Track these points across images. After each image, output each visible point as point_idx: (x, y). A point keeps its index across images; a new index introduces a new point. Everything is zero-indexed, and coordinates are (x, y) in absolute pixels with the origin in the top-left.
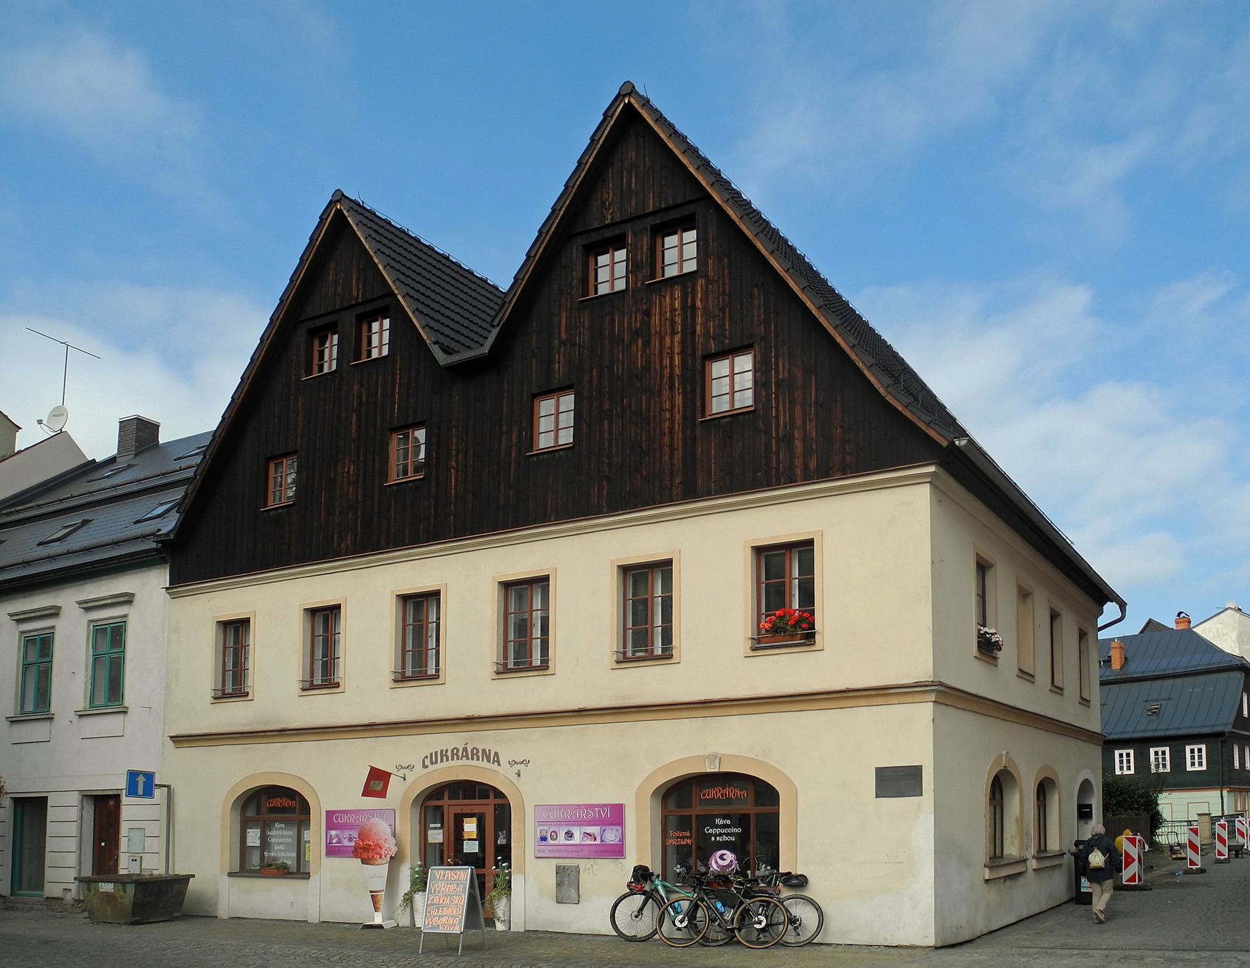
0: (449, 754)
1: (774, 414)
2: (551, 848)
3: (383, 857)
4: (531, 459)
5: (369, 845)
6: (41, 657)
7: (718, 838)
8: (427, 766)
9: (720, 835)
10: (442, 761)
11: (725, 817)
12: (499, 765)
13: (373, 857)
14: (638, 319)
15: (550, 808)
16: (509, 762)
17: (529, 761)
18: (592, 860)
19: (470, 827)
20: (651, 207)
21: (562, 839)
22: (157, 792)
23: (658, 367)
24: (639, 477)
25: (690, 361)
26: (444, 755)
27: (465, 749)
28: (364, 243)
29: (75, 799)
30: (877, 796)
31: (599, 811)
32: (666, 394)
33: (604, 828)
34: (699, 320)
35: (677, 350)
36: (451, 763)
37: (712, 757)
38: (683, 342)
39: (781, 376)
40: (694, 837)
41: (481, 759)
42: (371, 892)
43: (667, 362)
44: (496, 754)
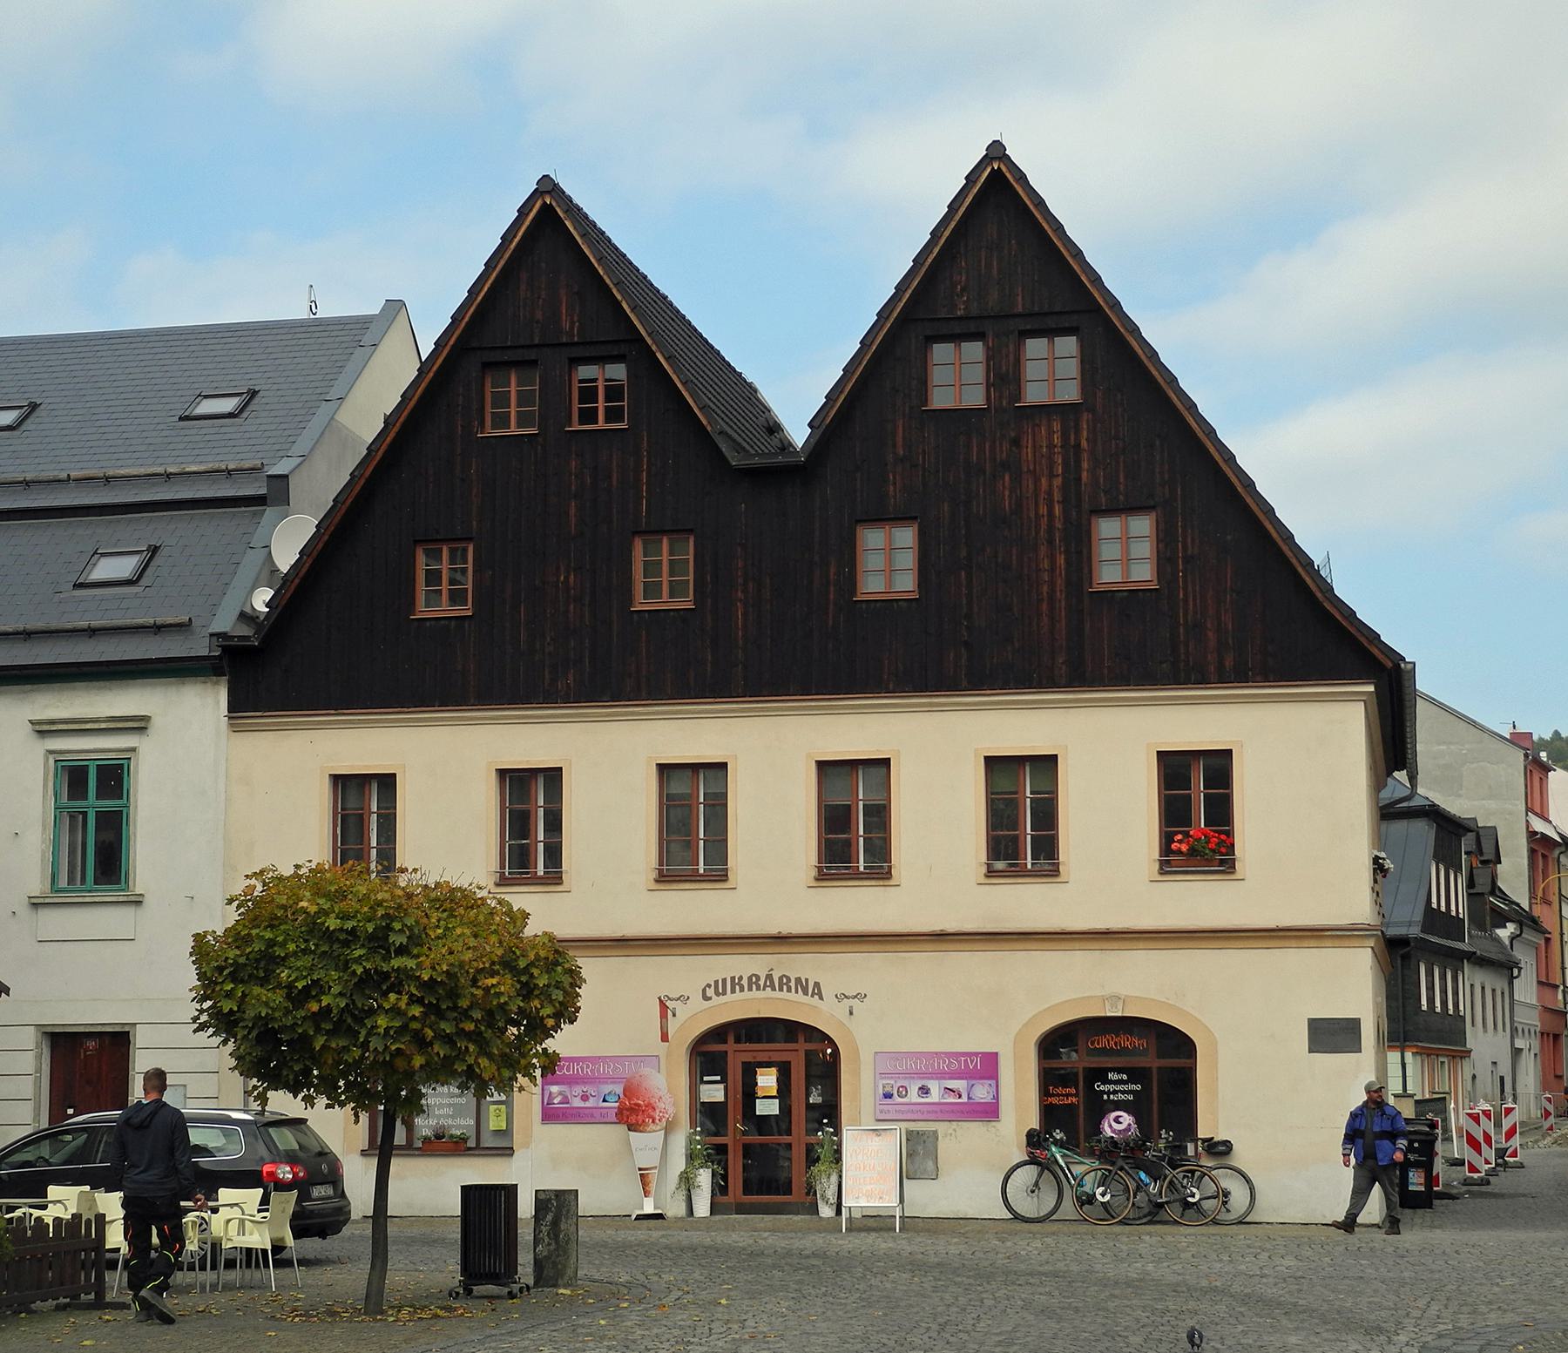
0: (745, 982)
1: (1181, 596)
2: (898, 1107)
3: (657, 1121)
4: (858, 606)
5: (639, 1105)
6: (86, 812)
7: (1112, 1096)
8: (710, 998)
9: (1115, 1092)
10: (733, 991)
11: (1119, 1071)
12: (821, 998)
13: (643, 1121)
14: (1004, 448)
15: (898, 1056)
16: (836, 996)
17: (865, 995)
18: (954, 1123)
19: (767, 1080)
20: (1020, 306)
21: (914, 1096)
23: (1032, 515)
24: (1009, 648)
25: (1074, 513)
26: (736, 983)
27: (770, 977)
28: (596, 265)
29: (29, 1038)
30: (1311, 1051)
31: (966, 1061)
32: (1043, 550)
33: (974, 1082)
34: (1085, 465)
35: (1057, 496)
36: (747, 994)
37: (1113, 998)
38: (1064, 488)
39: (1189, 552)
40: (1081, 1094)
41: (793, 990)
42: (640, 1169)
43: (1043, 510)
44: (817, 985)
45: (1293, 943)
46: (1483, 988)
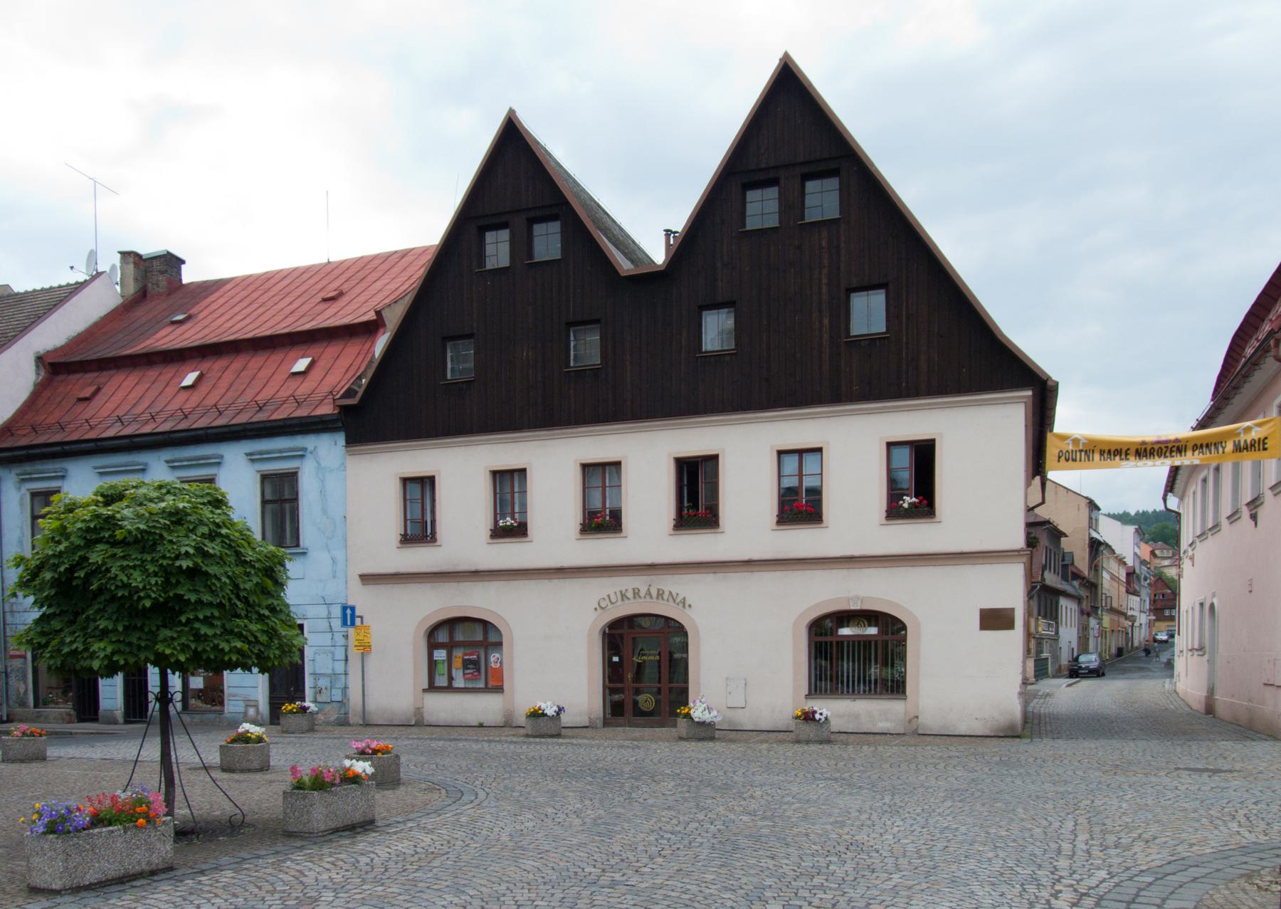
45: (981, 561)
46: (1066, 608)
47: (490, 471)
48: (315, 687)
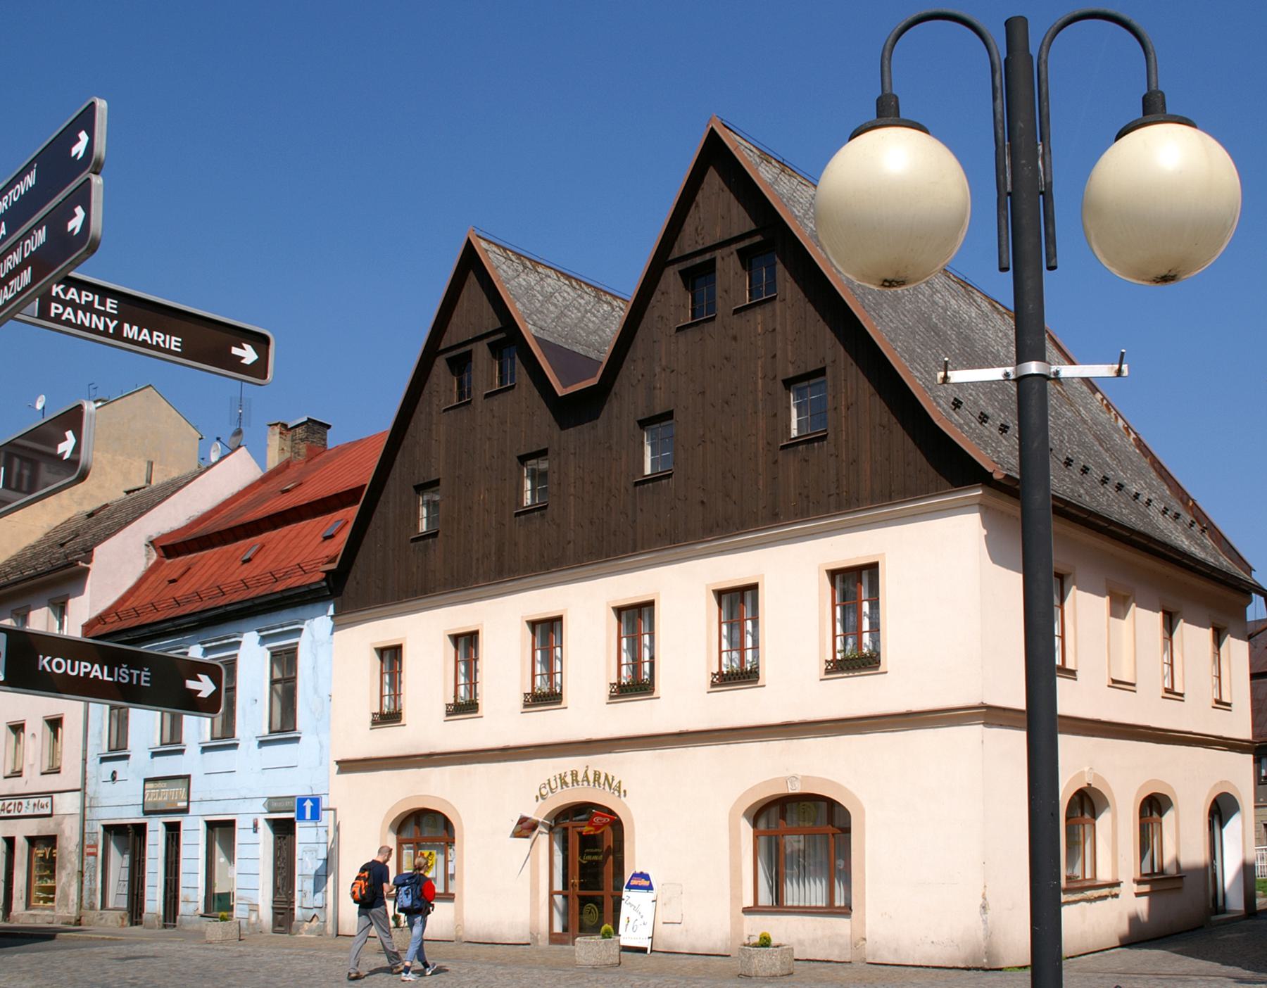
22: (324, 815)
47: (827, 571)
48: (302, 891)
